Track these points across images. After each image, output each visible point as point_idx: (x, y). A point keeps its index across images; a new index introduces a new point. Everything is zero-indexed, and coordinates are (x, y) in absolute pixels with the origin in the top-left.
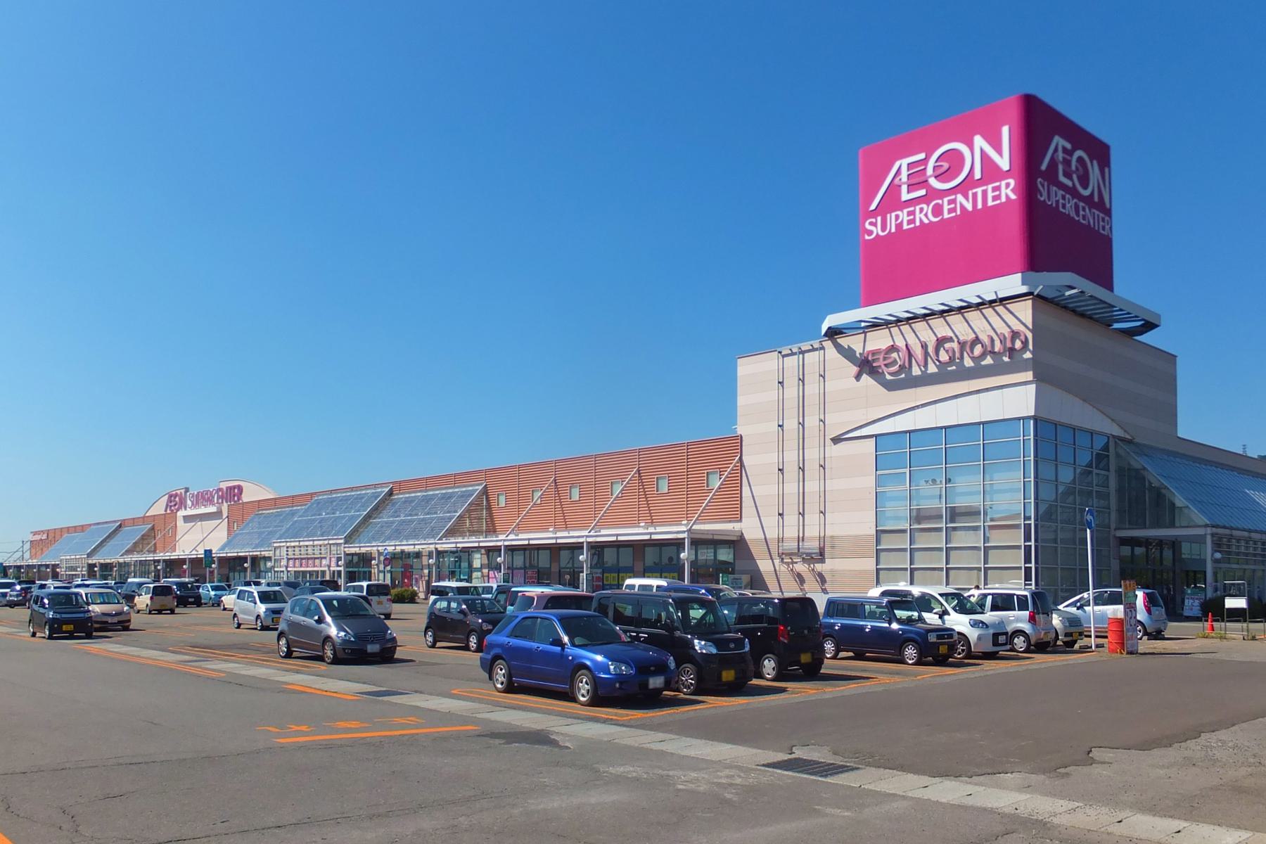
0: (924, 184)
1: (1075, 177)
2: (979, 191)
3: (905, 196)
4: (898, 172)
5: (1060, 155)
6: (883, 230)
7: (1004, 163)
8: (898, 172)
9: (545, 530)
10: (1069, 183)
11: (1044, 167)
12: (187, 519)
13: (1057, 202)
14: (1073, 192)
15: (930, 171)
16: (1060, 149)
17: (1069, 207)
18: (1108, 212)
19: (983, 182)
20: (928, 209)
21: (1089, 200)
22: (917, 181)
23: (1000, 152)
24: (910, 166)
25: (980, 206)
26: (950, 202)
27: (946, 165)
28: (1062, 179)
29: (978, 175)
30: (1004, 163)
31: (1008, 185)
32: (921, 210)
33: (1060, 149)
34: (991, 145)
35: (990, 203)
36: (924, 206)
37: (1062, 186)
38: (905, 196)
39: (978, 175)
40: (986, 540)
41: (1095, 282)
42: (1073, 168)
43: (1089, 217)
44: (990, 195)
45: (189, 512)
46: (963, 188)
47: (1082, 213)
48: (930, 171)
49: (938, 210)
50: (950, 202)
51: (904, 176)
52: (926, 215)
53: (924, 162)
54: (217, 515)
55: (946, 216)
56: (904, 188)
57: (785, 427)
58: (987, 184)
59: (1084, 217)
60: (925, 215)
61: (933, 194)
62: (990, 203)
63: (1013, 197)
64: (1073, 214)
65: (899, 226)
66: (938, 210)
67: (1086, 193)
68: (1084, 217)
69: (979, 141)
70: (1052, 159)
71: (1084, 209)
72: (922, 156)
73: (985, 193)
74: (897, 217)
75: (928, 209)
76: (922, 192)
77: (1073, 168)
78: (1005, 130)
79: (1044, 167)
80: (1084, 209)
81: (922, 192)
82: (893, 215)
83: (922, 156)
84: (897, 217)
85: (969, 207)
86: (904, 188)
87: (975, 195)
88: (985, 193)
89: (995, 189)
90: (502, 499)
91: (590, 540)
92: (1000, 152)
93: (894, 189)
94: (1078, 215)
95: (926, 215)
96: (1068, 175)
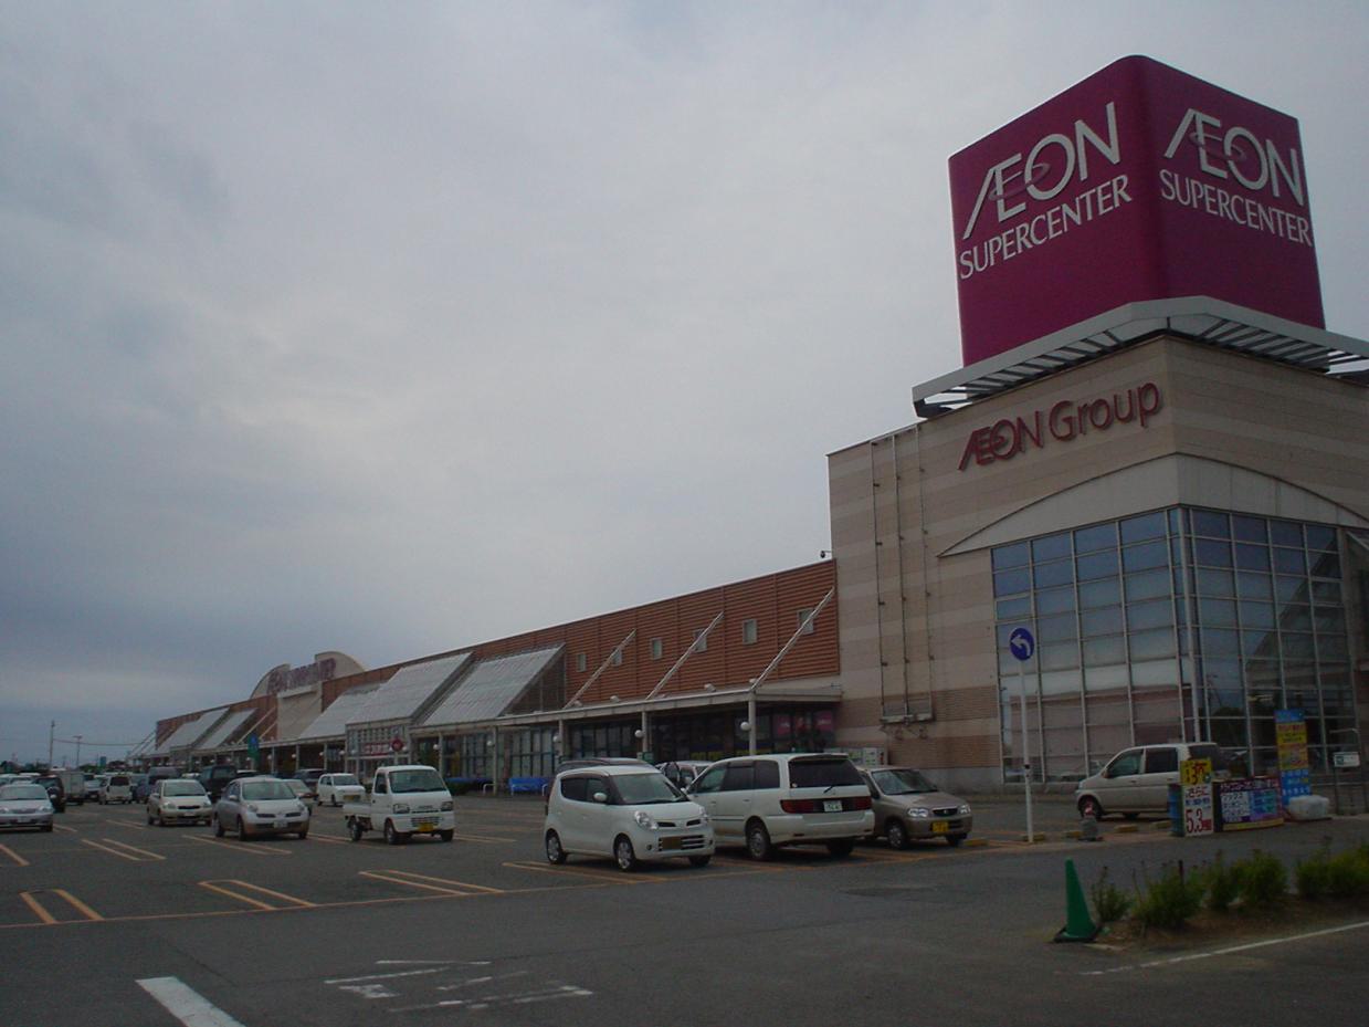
0: (1023, 195)
1: (1231, 164)
2: (1087, 195)
3: (1003, 215)
4: (993, 184)
5: (1201, 135)
6: (981, 266)
7: (1112, 154)
8: (993, 184)
9: (701, 689)
10: (1223, 174)
11: (1170, 153)
12: (286, 699)
13: (1201, 202)
14: (1232, 185)
15: (1028, 177)
16: (1200, 126)
17: (1226, 206)
18: (1304, 211)
19: (1092, 182)
20: (1029, 228)
21: (1264, 196)
22: (1015, 192)
23: (1107, 142)
24: (1005, 172)
25: (1090, 218)
26: (1055, 216)
27: (1046, 166)
28: (1206, 167)
29: (1084, 175)
30: (1112, 154)
31: (1120, 183)
32: (1023, 230)
33: (1200, 126)
34: (1096, 131)
35: (1102, 212)
36: (1026, 225)
37: (1207, 178)
38: (1003, 215)
39: (1084, 175)
40: (526, 755)
41: (1091, 316)
42: (1228, 152)
43: (1267, 219)
44: (1101, 199)
45: (289, 693)
46: (1067, 196)
47: (1249, 213)
48: (1028, 177)
49: (1041, 230)
50: (1055, 216)
51: (999, 190)
52: (1028, 237)
53: (1021, 165)
54: (313, 693)
55: (1052, 236)
56: (1001, 203)
57: (897, 538)
58: (1095, 186)
59: (1255, 220)
60: (1027, 238)
61: (1036, 207)
62: (1102, 212)
63: (1128, 199)
64: (1233, 216)
65: (999, 256)
66: (1041, 230)
67: (1258, 185)
68: (1255, 220)
69: (1081, 128)
70: (1186, 138)
71: (1254, 209)
72: (1018, 158)
73: (1094, 197)
74: (996, 243)
75: (1029, 228)
76: (1022, 207)
77: (1228, 152)
78: (1110, 107)
79: (1170, 153)
80: (1254, 209)
81: (1022, 207)
82: (991, 241)
83: (1018, 158)
84: (996, 243)
85: (1077, 219)
86: (1001, 203)
87: (1083, 202)
88: (1094, 197)
89: (1105, 191)
90: (659, 648)
91: (648, 708)
92: (1107, 142)
93: (989, 206)
94: (1244, 217)
95: (1028, 237)
96: (1218, 159)
